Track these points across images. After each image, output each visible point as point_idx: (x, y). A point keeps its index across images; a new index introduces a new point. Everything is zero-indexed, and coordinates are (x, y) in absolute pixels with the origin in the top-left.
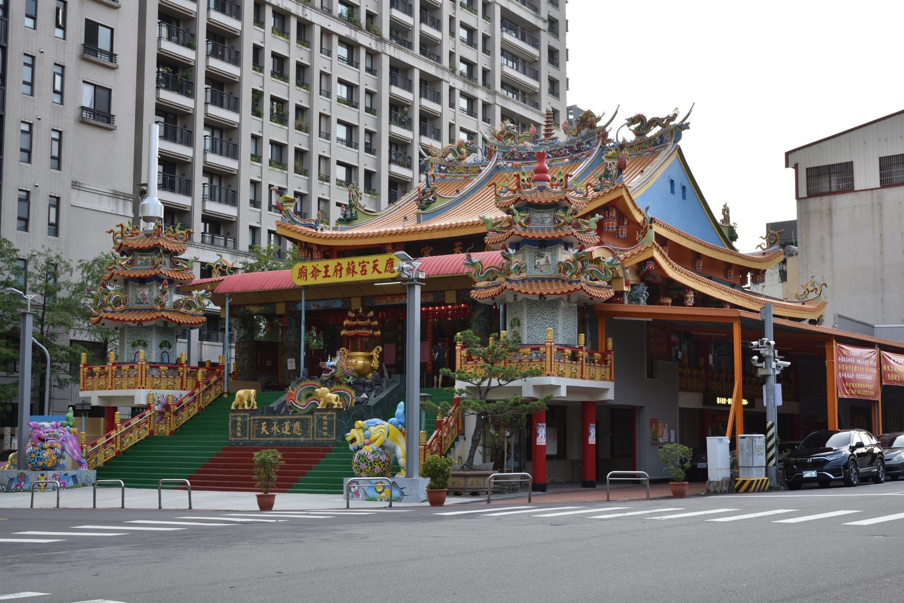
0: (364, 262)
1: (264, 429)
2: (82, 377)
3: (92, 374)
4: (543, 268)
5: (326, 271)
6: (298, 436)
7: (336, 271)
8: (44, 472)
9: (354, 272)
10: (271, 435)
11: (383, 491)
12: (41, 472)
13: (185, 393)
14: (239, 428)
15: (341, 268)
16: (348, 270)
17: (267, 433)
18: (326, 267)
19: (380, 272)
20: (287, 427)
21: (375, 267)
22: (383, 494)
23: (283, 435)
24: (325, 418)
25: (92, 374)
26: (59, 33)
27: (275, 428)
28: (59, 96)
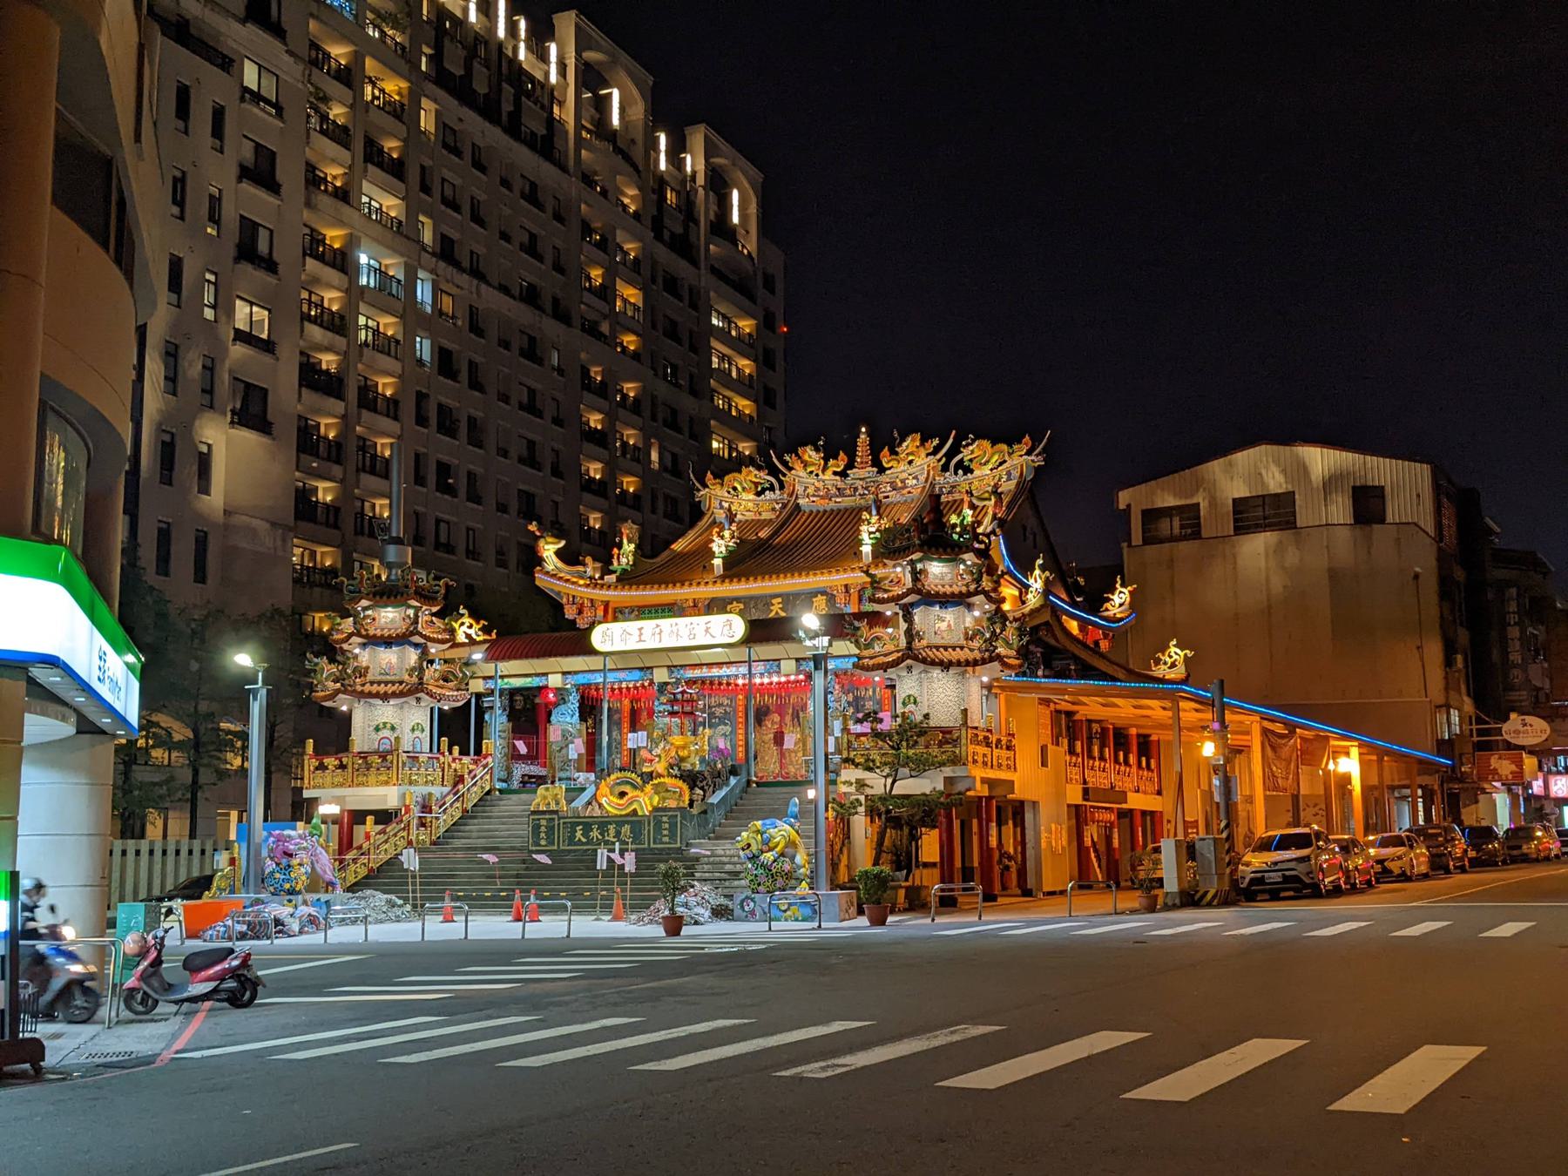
1: (579, 834)
3: (322, 767)
13: (446, 790)
20: (612, 831)
21: (707, 630)
25: (322, 767)
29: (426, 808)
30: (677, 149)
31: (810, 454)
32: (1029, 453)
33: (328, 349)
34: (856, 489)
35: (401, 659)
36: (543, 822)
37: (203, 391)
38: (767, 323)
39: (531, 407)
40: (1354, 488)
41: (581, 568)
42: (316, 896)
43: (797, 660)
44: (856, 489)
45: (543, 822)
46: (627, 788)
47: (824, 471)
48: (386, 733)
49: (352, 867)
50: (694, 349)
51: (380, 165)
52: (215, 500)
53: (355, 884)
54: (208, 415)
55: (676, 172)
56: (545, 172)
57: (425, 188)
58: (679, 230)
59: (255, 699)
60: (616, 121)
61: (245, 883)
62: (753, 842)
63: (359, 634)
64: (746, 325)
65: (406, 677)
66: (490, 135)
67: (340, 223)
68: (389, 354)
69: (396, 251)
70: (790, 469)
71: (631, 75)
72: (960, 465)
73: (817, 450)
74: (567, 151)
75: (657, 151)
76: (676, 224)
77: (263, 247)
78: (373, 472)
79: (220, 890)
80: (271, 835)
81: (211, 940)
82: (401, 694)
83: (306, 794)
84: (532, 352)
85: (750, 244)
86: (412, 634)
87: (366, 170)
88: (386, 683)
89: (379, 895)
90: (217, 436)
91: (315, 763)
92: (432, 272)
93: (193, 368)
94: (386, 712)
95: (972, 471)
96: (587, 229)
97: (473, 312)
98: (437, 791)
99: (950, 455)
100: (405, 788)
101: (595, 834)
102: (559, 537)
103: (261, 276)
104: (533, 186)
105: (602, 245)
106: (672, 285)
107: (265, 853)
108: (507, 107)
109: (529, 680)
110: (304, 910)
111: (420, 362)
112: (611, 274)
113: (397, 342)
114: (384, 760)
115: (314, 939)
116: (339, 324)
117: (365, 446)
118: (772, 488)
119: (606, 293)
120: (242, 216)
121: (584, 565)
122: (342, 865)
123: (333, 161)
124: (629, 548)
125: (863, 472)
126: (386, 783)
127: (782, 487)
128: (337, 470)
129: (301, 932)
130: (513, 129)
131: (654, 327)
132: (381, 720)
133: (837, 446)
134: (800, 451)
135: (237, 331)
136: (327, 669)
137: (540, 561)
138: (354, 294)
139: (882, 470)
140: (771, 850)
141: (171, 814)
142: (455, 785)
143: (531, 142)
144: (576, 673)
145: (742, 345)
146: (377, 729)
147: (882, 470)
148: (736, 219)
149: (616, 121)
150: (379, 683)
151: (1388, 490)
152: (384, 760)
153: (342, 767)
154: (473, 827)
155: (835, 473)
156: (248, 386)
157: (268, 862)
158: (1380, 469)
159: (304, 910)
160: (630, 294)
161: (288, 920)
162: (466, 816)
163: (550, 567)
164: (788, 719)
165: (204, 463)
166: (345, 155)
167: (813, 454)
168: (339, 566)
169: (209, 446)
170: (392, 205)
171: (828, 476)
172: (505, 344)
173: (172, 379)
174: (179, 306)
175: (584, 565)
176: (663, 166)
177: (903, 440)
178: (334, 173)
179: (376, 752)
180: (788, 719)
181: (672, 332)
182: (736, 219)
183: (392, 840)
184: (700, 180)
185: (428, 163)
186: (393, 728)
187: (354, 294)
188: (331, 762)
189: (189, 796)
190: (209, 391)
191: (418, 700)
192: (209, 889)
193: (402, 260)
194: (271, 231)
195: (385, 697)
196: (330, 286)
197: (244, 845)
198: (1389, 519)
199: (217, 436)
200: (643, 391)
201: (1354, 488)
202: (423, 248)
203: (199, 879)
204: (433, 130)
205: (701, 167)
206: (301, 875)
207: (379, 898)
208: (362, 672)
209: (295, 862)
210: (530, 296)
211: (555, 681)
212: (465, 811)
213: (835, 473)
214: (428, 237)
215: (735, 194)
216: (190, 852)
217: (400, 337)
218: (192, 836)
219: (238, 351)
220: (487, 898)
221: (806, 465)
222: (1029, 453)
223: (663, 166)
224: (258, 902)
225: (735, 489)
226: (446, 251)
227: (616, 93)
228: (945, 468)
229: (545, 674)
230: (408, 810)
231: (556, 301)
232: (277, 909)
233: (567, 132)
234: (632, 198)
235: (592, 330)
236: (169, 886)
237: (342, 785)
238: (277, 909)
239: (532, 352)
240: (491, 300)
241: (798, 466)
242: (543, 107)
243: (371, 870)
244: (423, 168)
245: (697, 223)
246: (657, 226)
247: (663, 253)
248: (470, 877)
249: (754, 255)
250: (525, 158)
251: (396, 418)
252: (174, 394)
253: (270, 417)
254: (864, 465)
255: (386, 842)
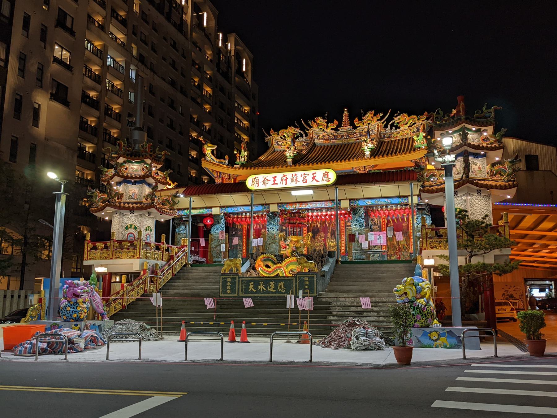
0: (304, 174)
1: (251, 287)
2: (86, 251)
3: (95, 248)
4: (477, 173)
5: (275, 180)
6: (282, 293)
7: (282, 180)
8: (77, 323)
9: (297, 181)
10: (258, 291)
11: (438, 339)
12: (75, 323)
13: (164, 263)
14: (229, 287)
15: (287, 179)
16: (292, 180)
17: (255, 291)
18: (274, 178)
19: (318, 181)
20: (272, 286)
21: (314, 178)
22: (438, 342)
23: (269, 292)
24: (306, 279)
25: (95, 248)
26: (43, 44)
27: (261, 287)
28: (40, 82)
29: (154, 272)
30: (225, 41)
31: (320, 120)
32: (427, 119)
33: (93, 89)
34: (343, 136)
35: (141, 191)
36: (229, 280)
37: (37, 79)
38: (253, 110)
39: (171, 126)
40: (526, 156)
41: (223, 161)
42: (93, 322)
43: (350, 200)
44: (343, 136)
45: (229, 280)
46: (270, 264)
47: (327, 127)
48: (131, 231)
49: (113, 305)
50: (229, 114)
51: (117, 18)
52: (42, 129)
53: (114, 315)
54: (39, 90)
55: (224, 49)
56: (180, 37)
57: (134, 34)
58: (225, 70)
59: (59, 201)
60: (205, 24)
61: (48, 313)
62: (408, 291)
63: (118, 175)
64: (246, 109)
65: (144, 200)
66: (160, 19)
67: (100, 38)
68: (118, 95)
69: (123, 55)
70: (311, 127)
71: (209, 6)
72: (392, 125)
73: (324, 119)
74: (187, 31)
75: (219, 40)
76: (224, 66)
77: (68, 23)
78: (109, 142)
79: (31, 317)
80: (66, 283)
81: (20, 354)
82: (142, 209)
83: (85, 263)
84: (172, 105)
85: (249, 79)
86: (148, 176)
87: (111, 20)
88: (132, 203)
89: (135, 322)
90: (42, 100)
91: (91, 245)
92: (136, 66)
93: (33, 67)
94: (132, 219)
95: (399, 128)
96: (194, 64)
97: (151, 86)
98: (160, 263)
99: (388, 121)
100: (143, 260)
101: (261, 287)
102: (214, 144)
103: (66, 35)
104: (175, 43)
105: (199, 69)
106: (222, 90)
107: (60, 295)
108: (166, 10)
109: (202, 210)
110: (88, 333)
111: (130, 102)
112: (202, 80)
113: (121, 91)
114: (131, 245)
115: (96, 355)
116: (98, 79)
117: (107, 133)
118: (302, 136)
119: (200, 87)
120: (59, 8)
121: (225, 159)
122: (107, 303)
123: (98, 13)
124: (244, 153)
125: (345, 129)
126: (133, 257)
127: (306, 135)
128: (96, 140)
129: (86, 348)
130: (168, 18)
131: (216, 103)
132: (129, 224)
133: (333, 116)
134: (315, 119)
135: (54, 57)
136: (99, 196)
137: (204, 155)
138: (104, 67)
139: (355, 127)
140: (422, 297)
141: (12, 279)
142: (168, 261)
143: (175, 25)
144: (227, 207)
145: (246, 116)
146: (127, 228)
147: (355, 127)
148: (244, 70)
149: (205, 24)
150: (128, 203)
151: (539, 157)
152: (131, 245)
153: (106, 247)
154: (179, 283)
155: (332, 129)
156: (59, 85)
157: (63, 300)
158: (536, 149)
159: (88, 333)
160: (208, 90)
161: (77, 340)
162: (175, 278)
163: (209, 159)
164: (329, 235)
165: (36, 112)
166: (103, 12)
167: (322, 120)
168: (94, 179)
169: (39, 105)
170: (121, 36)
171: (329, 130)
172: (163, 100)
173: (22, 71)
174: (27, 37)
175: (225, 159)
176: (220, 45)
177: (365, 114)
178: (99, 19)
179: (126, 240)
180: (329, 235)
181: (222, 106)
182: (244, 70)
183: (136, 290)
184: (233, 53)
185: (135, 23)
186: (135, 228)
187: (104, 67)
188: (100, 245)
189: (20, 268)
190: (40, 79)
191: (149, 213)
192: (25, 316)
193: (124, 59)
194: (73, 18)
195: (132, 210)
196: (96, 64)
197: (48, 291)
198: (540, 169)
199: (42, 100)
200: (212, 126)
201: (526, 156)
202: (134, 57)
203: (23, 310)
204: (138, 11)
205: (233, 49)
206: (84, 308)
207: (135, 325)
208: (120, 196)
209: (80, 300)
210: (173, 83)
211: (216, 211)
212: (173, 275)
213: (332, 129)
214: (134, 53)
215: (244, 61)
216: (19, 297)
217: (123, 89)
218: (21, 288)
219: (55, 67)
220: (211, 326)
221: (318, 125)
222: (427, 119)
223: (220, 45)
224: (55, 326)
225: (284, 136)
226: (141, 59)
227: (205, 14)
228: (386, 126)
229: (211, 208)
230: (145, 272)
231: (182, 88)
232: (69, 332)
233: (187, 25)
234: (209, 55)
235: (194, 100)
236: (7, 313)
237: (106, 258)
238: (69, 332)
239: (172, 105)
240: (158, 81)
241: (314, 125)
242: (179, 13)
243: (124, 307)
244: (134, 26)
245: (231, 68)
246: (218, 65)
247: (220, 78)
248: (185, 311)
249: (250, 84)
250: (172, 30)
251: (119, 121)
252: (23, 77)
253: (69, 100)
254: (346, 125)
255: (133, 290)
